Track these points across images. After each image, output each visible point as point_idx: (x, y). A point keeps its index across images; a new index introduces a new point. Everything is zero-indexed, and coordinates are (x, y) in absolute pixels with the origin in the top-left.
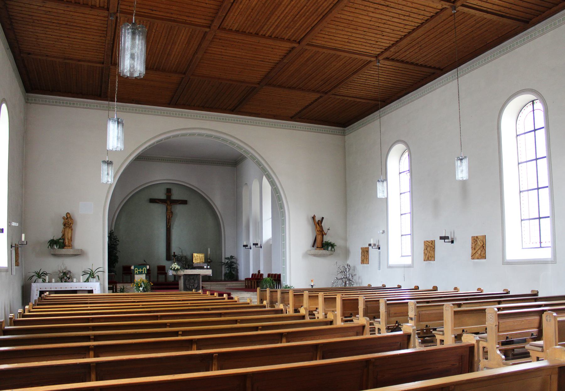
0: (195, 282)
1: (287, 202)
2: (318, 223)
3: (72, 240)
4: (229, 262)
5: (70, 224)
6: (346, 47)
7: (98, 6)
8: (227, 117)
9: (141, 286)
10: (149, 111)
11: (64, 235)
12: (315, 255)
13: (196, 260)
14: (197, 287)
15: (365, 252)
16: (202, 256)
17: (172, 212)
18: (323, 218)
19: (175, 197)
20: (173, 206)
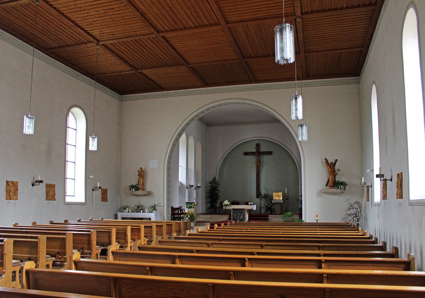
5: (142, 175)
6: (258, 16)
7: (213, 24)
9: (187, 217)
10: (152, 96)
11: (138, 182)
18: (336, 160)
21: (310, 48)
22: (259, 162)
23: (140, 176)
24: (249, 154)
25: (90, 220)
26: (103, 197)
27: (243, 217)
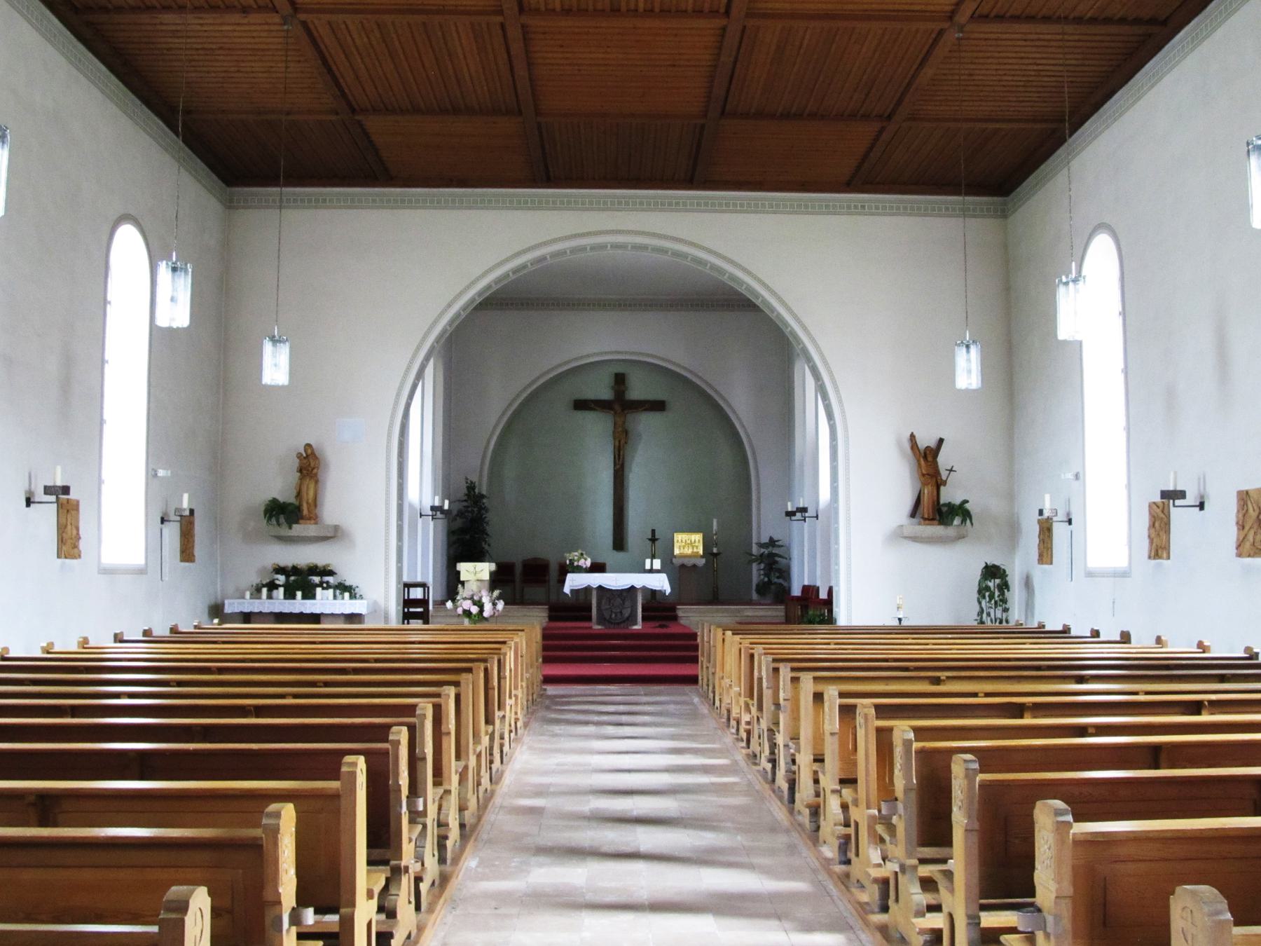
0: (624, 604)
1: (840, 401)
2: (925, 457)
3: (318, 503)
4: (766, 552)
5: (314, 468)
8: (638, 197)
12: (915, 539)
13: (682, 549)
14: (629, 616)
15: (1046, 529)
16: (697, 538)
17: (626, 432)
18: (941, 441)
19: (637, 392)
20: (628, 416)
21: (924, 108)
22: (625, 434)
23: (305, 472)
24: (593, 406)
25: (196, 627)
26: (184, 544)
27: (631, 613)
